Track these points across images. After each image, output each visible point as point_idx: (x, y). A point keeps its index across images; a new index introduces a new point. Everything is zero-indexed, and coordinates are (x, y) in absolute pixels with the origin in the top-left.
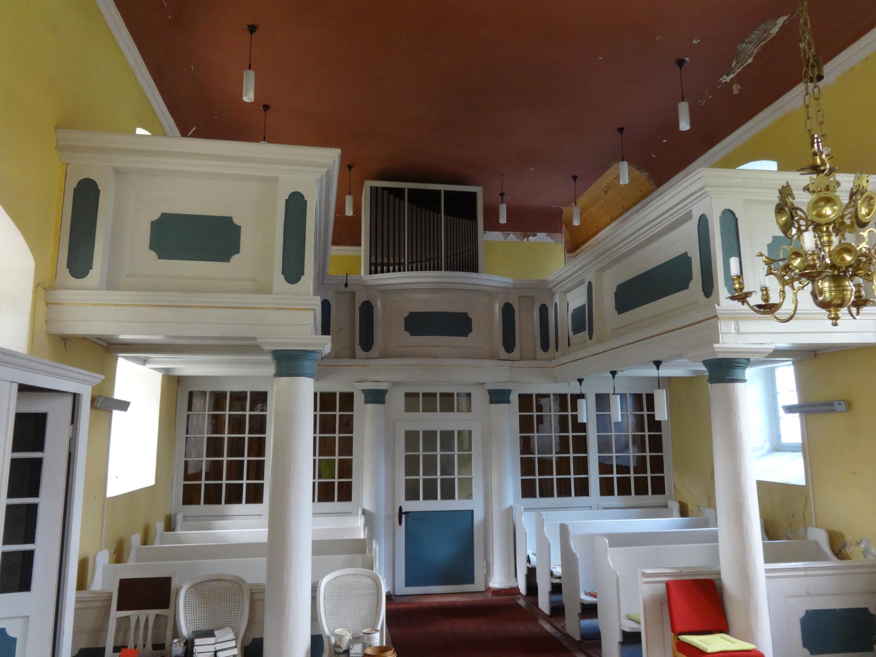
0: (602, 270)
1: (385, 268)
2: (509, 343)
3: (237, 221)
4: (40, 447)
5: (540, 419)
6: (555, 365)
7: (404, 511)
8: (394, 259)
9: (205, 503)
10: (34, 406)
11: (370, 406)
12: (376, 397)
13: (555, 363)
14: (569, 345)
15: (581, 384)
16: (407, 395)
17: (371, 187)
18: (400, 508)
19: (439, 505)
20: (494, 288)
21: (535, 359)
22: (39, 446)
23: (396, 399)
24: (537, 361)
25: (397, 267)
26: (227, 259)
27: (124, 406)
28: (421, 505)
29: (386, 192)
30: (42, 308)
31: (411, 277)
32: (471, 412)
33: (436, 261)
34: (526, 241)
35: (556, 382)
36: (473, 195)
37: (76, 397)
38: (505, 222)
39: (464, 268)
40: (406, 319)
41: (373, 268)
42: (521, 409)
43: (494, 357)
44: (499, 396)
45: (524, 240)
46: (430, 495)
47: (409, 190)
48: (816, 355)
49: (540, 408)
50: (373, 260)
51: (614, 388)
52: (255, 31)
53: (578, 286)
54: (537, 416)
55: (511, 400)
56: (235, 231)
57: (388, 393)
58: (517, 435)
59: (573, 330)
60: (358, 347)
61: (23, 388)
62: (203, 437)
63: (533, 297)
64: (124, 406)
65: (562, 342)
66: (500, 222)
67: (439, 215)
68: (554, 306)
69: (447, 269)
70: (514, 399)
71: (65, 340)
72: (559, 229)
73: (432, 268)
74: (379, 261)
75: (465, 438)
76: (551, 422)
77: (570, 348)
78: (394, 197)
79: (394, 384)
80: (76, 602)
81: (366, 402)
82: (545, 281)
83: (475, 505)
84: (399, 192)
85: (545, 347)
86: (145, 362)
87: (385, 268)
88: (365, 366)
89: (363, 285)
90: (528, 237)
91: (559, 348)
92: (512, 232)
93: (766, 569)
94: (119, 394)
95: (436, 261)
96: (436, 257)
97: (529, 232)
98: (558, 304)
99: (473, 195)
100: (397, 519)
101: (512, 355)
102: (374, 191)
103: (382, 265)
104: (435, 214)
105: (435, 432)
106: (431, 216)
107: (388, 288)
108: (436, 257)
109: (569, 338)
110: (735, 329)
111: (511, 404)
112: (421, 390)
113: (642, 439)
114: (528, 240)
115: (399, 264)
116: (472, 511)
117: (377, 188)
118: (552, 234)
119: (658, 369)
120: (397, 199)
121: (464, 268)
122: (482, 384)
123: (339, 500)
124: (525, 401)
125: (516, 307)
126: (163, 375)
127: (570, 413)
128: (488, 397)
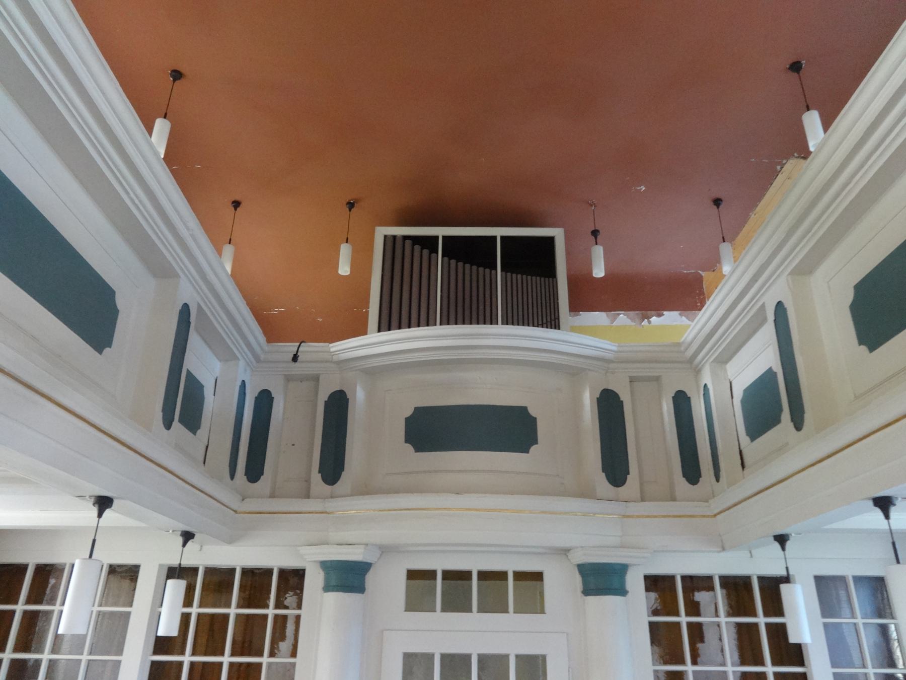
0: (805, 269)
3: (409, 448)
5: (697, 632)
6: (716, 511)
11: (333, 597)
13: (716, 505)
14: (743, 466)
15: (783, 549)
17: (385, 236)
20: (582, 360)
21: (673, 499)
24: (678, 503)
29: (408, 242)
32: (544, 613)
34: (647, 324)
35: (723, 549)
39: (515, 318)
43: (586, 493)
45: (642, 324)
49: (693, 608)
51: (894, 544)
53: (755, 332)
54: (690, 625)
57: (371, 570)
59: (748, 434)
60: (316, 477)
62: (90, 653)
63: (657, 379)
65: (729, 460)
67: (493, 272)
68: (702, 392)
70: (635, 582)
72: (699, 304)
76: (720, 640)
77: (745, 472)
78: (422, 249)
79: (385, 550)
81: (328, 588)
82: (679, 345)
84: (429, 243)
85: (692, 473)
88: (326, 513)
89: (331, 362)
90: (648, 318)
91: (723, 473)
92: (623, 312)
97: (651, 310)
98: (710, 386)
102: (391, 242)
104: (487, 270)
107: (375, 362)
109: (741, 452)
112: (440, 564)
113: (452, 579)
114: (649, 322)
117: (394, 237)
118: (689, 312)
120: (426, 252)
121: (515, 318)
125: (625, 397)
127: (761, 620)
128: (578, 579)
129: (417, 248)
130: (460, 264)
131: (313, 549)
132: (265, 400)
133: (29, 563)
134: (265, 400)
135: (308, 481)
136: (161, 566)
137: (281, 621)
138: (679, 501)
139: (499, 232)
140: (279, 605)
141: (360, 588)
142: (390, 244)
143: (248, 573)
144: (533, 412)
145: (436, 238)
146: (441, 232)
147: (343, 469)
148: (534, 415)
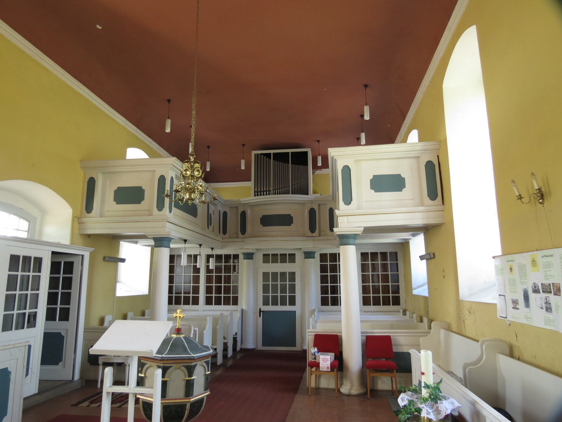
1: (262, 193)
2: (312, 228)
3: (143, 188)
4: (72, 273)
7: (262, 310)
8: (266, 189)
9: (175, 304)
10: (57, 260)
12: (249, 256)
16: (264, 255)
17: (255, 154)
18: (260, 309)
19: (279, 308)
20: (302, 201)
22: (71, 273)
23: (259, 257)
25: (268, 193)
26: (140, 203)
27: (123, 260)
28: (270, 308)
29: (262, 156)
30: (77, 226)
31: (264, 198)
33: (287, 188)
36: (306, 153)
37: (83, 256)
38: (321, 165)
40: (261, 219)
41: (256, 194)
42: (321, 261)
44: (309, 255)
46: (275, 303)
47: (273, 153)
48: (428, 230)
50: (256, 189)
52: (170, 101)
55: (315, 256)
56: (143, 192)
58: (319, 274)
60: (239, 233)
61: (53, 253)
64: (123, 260)
66: (318, 165)
67: (288, 164)
69: (292, 193)
70: (317, 256)
71: (89, 236)
73: (283, 193)
74: (259, 190)
75: (292, 275)
79: (257, 250)
80: (84, 329)
81: (244, 259)
83: (296, 308)
84: (268, 155)
86: (136, 243)
87: (262, 193)
93: (361, 332)
94: (122, 255)
95: (287, 188)
96: (287, 186)
99: (306, 153)
100: (258, 314)
101: (314, 234)
102: (257, 156)
103: (261, 192)
105: (269, 273)
106: (285, 166)
107: (253, 204)
108: (287, 186)
110: (347, 220)
111: (315, 259)
112: (271, 253)
115: (269, 191)
116: (295, 311)
119: (185, 243)
120: (268, 159)
122: (300, 249)
123: (232, 305)
124: (323, 257)
126: (151, 248)
128: (303, 255)
129: (265, 157)
130: (278, 162)
131: (241, 250)
132: (225, 214)
133: (205, 254)
134: (225, 214)
135: (237, 233)
136: (205, 254)
137: (234, 266)
138: (323, 236)
139: (290, 151)
140: (234, 263)
141: (252, 258)
142: (256, 156)
143: (188, 304)
144: (292, 215)
145: (270, 154)
146: (272, 152)
147: (246, 231)
148: (292, 216)
